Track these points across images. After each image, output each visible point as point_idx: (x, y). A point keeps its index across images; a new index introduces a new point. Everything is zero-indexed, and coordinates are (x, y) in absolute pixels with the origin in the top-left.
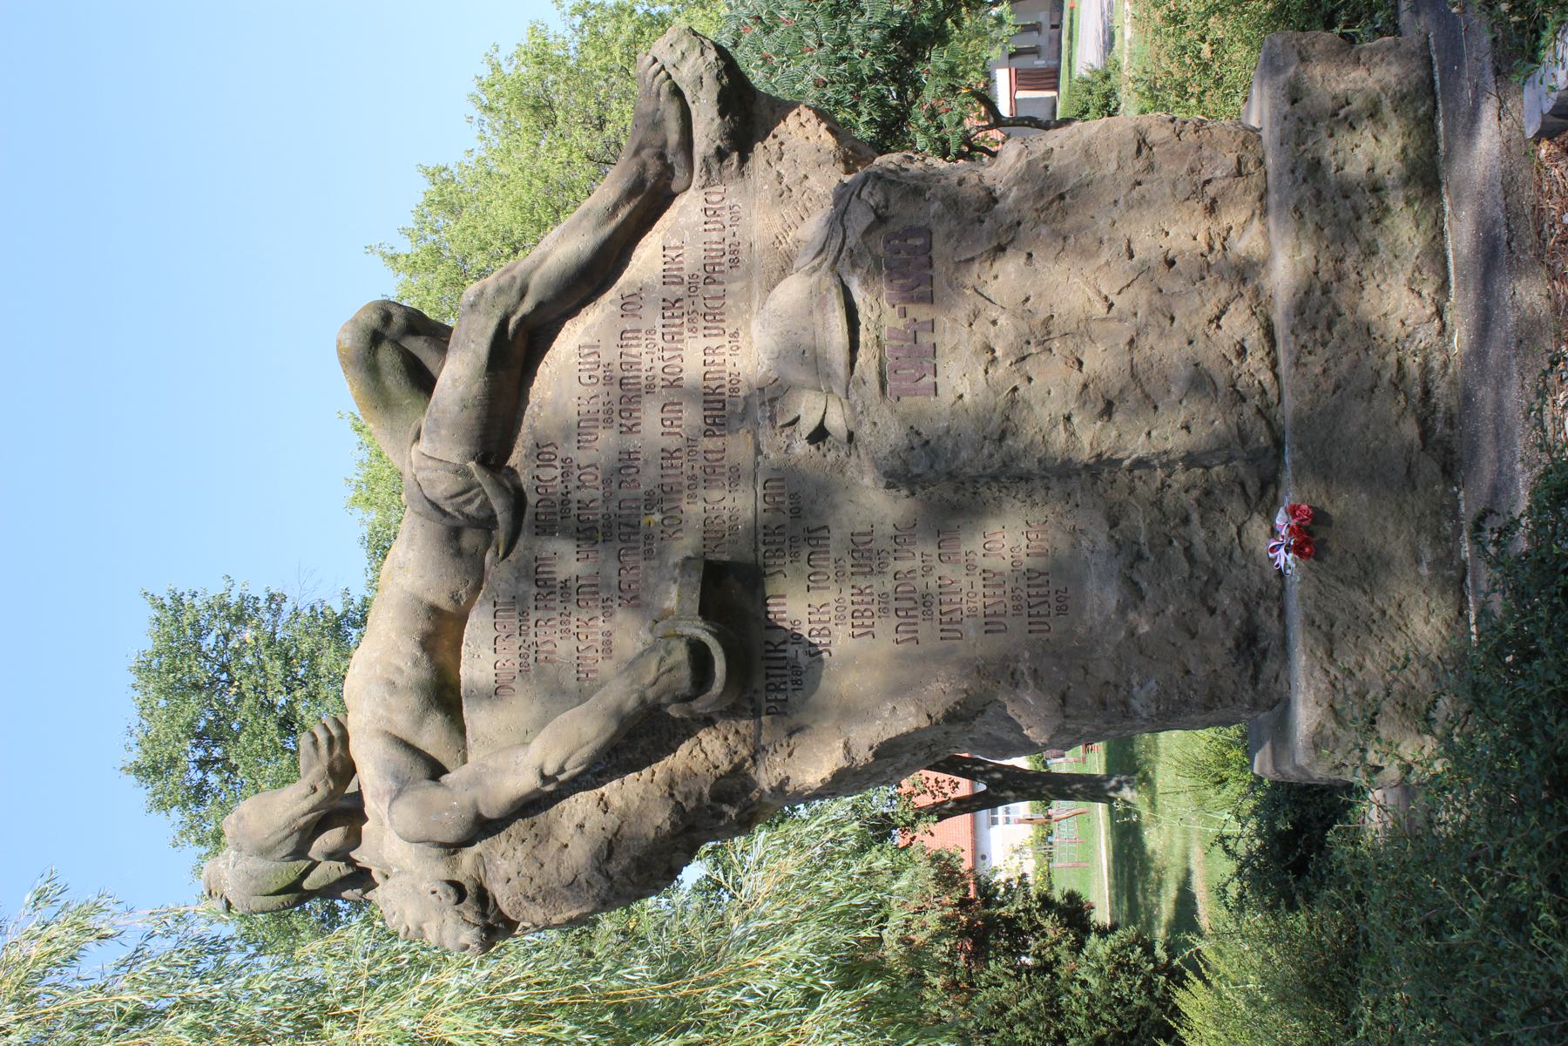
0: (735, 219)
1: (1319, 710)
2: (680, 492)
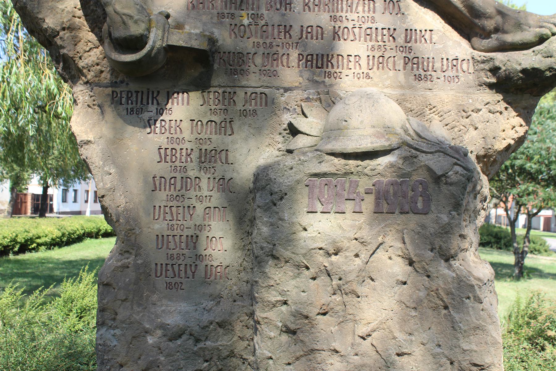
0: (450, 80)
2: (262, 37)
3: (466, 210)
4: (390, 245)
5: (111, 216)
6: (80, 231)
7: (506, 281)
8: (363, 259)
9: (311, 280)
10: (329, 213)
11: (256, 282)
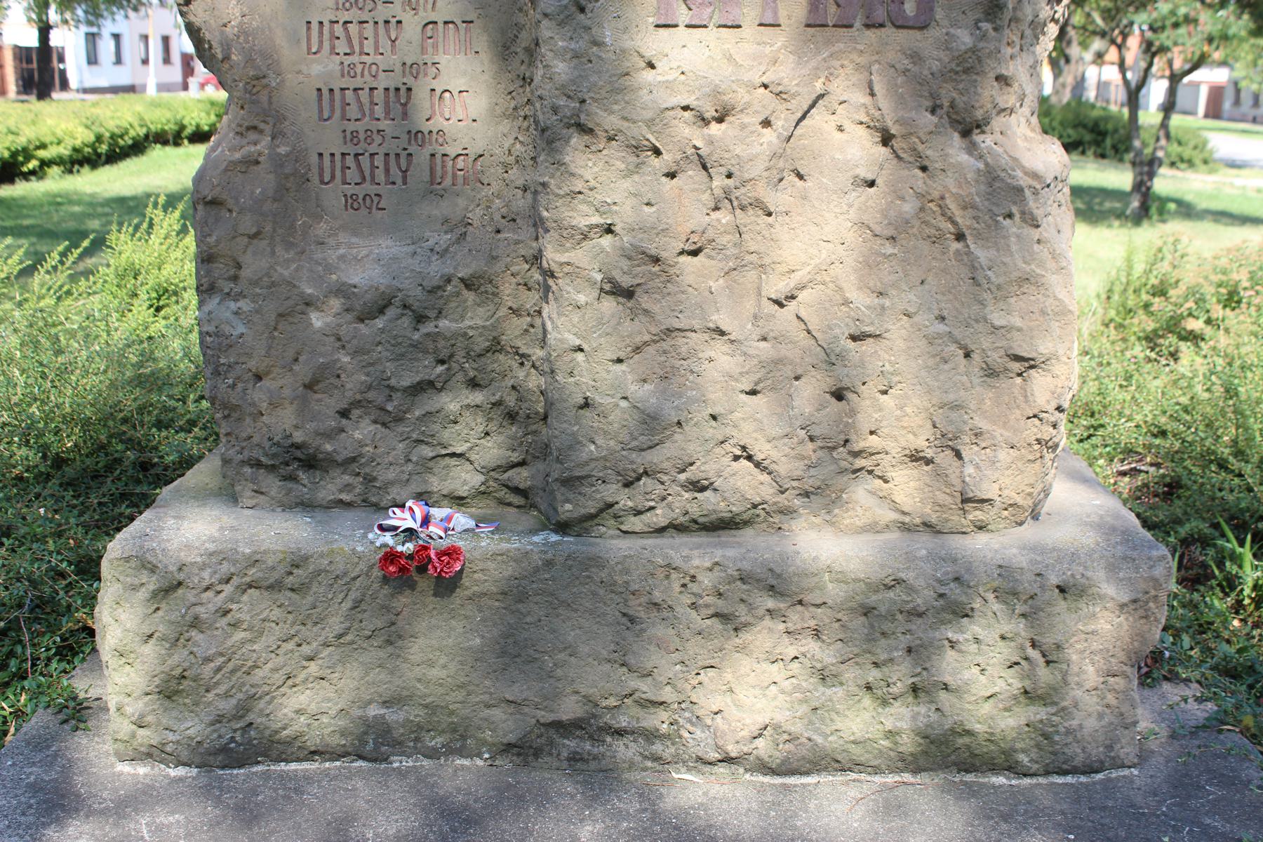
1: (173, 568)
3: (1015, 20)
4: (842, 99)
5: (211, 47)
6: (138, 129)
7: (1110, 226)
8: (781, 130)
9: (664, 179)
10: (705, 26)
11: (544, 185)
